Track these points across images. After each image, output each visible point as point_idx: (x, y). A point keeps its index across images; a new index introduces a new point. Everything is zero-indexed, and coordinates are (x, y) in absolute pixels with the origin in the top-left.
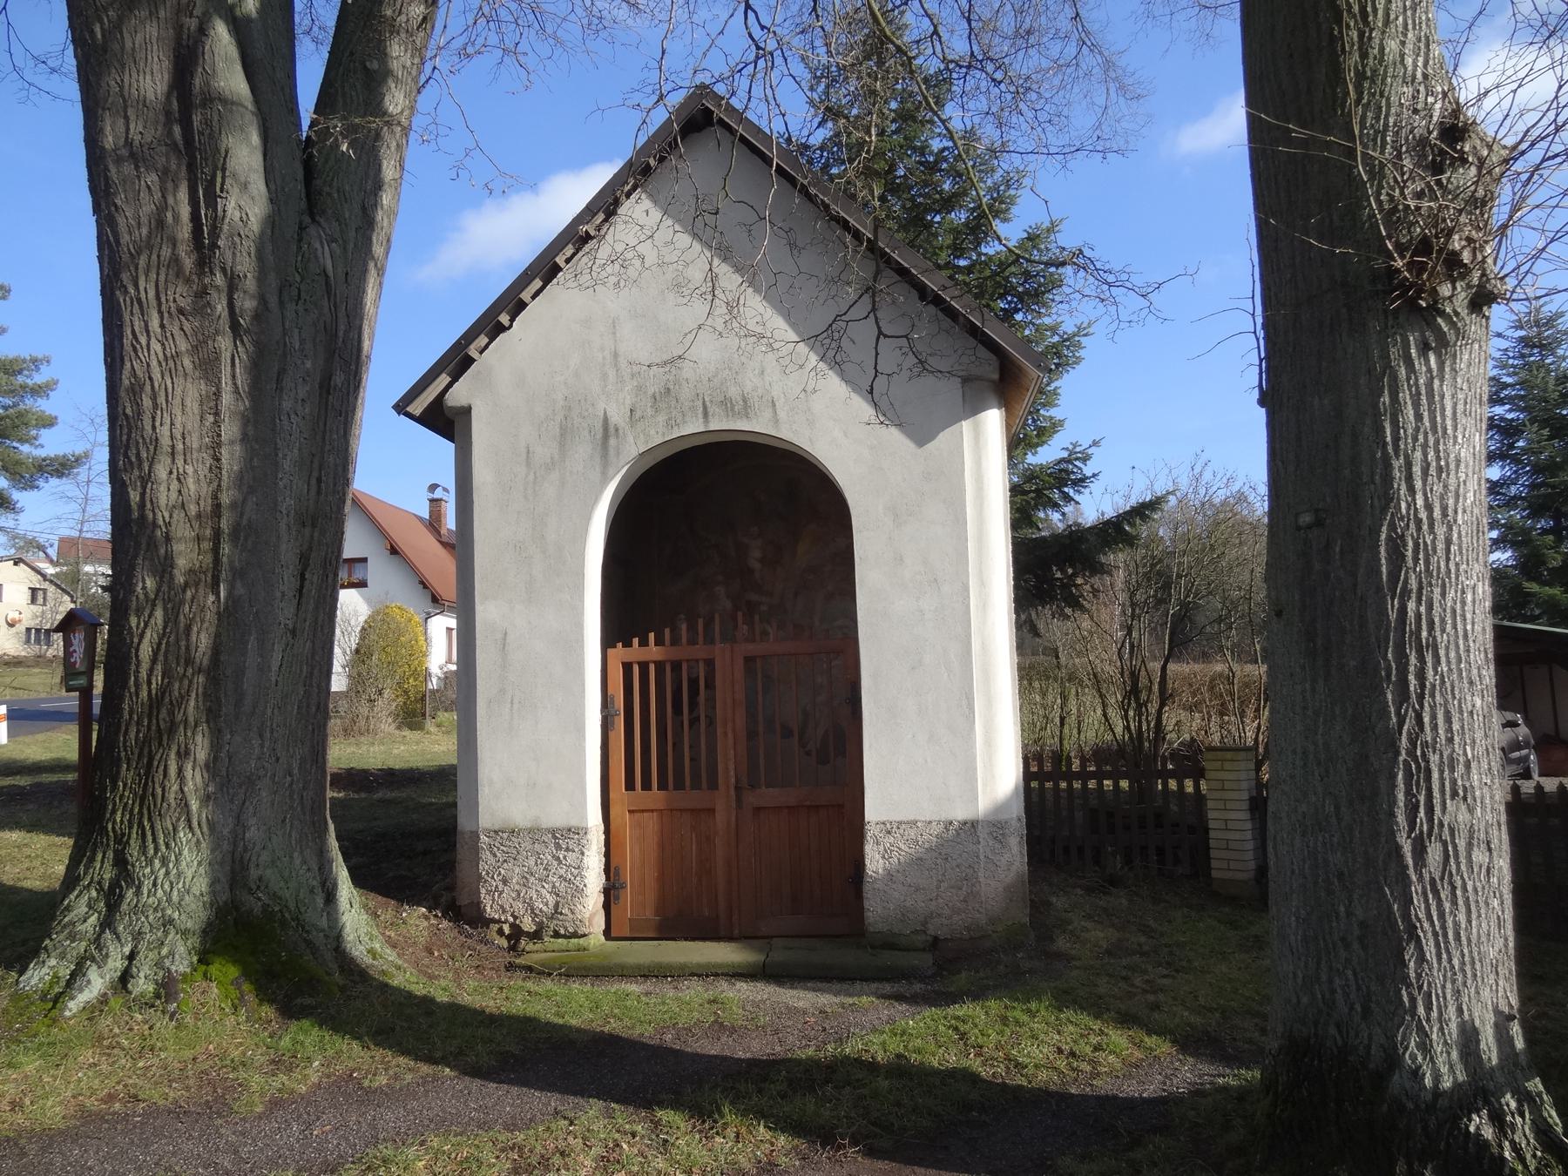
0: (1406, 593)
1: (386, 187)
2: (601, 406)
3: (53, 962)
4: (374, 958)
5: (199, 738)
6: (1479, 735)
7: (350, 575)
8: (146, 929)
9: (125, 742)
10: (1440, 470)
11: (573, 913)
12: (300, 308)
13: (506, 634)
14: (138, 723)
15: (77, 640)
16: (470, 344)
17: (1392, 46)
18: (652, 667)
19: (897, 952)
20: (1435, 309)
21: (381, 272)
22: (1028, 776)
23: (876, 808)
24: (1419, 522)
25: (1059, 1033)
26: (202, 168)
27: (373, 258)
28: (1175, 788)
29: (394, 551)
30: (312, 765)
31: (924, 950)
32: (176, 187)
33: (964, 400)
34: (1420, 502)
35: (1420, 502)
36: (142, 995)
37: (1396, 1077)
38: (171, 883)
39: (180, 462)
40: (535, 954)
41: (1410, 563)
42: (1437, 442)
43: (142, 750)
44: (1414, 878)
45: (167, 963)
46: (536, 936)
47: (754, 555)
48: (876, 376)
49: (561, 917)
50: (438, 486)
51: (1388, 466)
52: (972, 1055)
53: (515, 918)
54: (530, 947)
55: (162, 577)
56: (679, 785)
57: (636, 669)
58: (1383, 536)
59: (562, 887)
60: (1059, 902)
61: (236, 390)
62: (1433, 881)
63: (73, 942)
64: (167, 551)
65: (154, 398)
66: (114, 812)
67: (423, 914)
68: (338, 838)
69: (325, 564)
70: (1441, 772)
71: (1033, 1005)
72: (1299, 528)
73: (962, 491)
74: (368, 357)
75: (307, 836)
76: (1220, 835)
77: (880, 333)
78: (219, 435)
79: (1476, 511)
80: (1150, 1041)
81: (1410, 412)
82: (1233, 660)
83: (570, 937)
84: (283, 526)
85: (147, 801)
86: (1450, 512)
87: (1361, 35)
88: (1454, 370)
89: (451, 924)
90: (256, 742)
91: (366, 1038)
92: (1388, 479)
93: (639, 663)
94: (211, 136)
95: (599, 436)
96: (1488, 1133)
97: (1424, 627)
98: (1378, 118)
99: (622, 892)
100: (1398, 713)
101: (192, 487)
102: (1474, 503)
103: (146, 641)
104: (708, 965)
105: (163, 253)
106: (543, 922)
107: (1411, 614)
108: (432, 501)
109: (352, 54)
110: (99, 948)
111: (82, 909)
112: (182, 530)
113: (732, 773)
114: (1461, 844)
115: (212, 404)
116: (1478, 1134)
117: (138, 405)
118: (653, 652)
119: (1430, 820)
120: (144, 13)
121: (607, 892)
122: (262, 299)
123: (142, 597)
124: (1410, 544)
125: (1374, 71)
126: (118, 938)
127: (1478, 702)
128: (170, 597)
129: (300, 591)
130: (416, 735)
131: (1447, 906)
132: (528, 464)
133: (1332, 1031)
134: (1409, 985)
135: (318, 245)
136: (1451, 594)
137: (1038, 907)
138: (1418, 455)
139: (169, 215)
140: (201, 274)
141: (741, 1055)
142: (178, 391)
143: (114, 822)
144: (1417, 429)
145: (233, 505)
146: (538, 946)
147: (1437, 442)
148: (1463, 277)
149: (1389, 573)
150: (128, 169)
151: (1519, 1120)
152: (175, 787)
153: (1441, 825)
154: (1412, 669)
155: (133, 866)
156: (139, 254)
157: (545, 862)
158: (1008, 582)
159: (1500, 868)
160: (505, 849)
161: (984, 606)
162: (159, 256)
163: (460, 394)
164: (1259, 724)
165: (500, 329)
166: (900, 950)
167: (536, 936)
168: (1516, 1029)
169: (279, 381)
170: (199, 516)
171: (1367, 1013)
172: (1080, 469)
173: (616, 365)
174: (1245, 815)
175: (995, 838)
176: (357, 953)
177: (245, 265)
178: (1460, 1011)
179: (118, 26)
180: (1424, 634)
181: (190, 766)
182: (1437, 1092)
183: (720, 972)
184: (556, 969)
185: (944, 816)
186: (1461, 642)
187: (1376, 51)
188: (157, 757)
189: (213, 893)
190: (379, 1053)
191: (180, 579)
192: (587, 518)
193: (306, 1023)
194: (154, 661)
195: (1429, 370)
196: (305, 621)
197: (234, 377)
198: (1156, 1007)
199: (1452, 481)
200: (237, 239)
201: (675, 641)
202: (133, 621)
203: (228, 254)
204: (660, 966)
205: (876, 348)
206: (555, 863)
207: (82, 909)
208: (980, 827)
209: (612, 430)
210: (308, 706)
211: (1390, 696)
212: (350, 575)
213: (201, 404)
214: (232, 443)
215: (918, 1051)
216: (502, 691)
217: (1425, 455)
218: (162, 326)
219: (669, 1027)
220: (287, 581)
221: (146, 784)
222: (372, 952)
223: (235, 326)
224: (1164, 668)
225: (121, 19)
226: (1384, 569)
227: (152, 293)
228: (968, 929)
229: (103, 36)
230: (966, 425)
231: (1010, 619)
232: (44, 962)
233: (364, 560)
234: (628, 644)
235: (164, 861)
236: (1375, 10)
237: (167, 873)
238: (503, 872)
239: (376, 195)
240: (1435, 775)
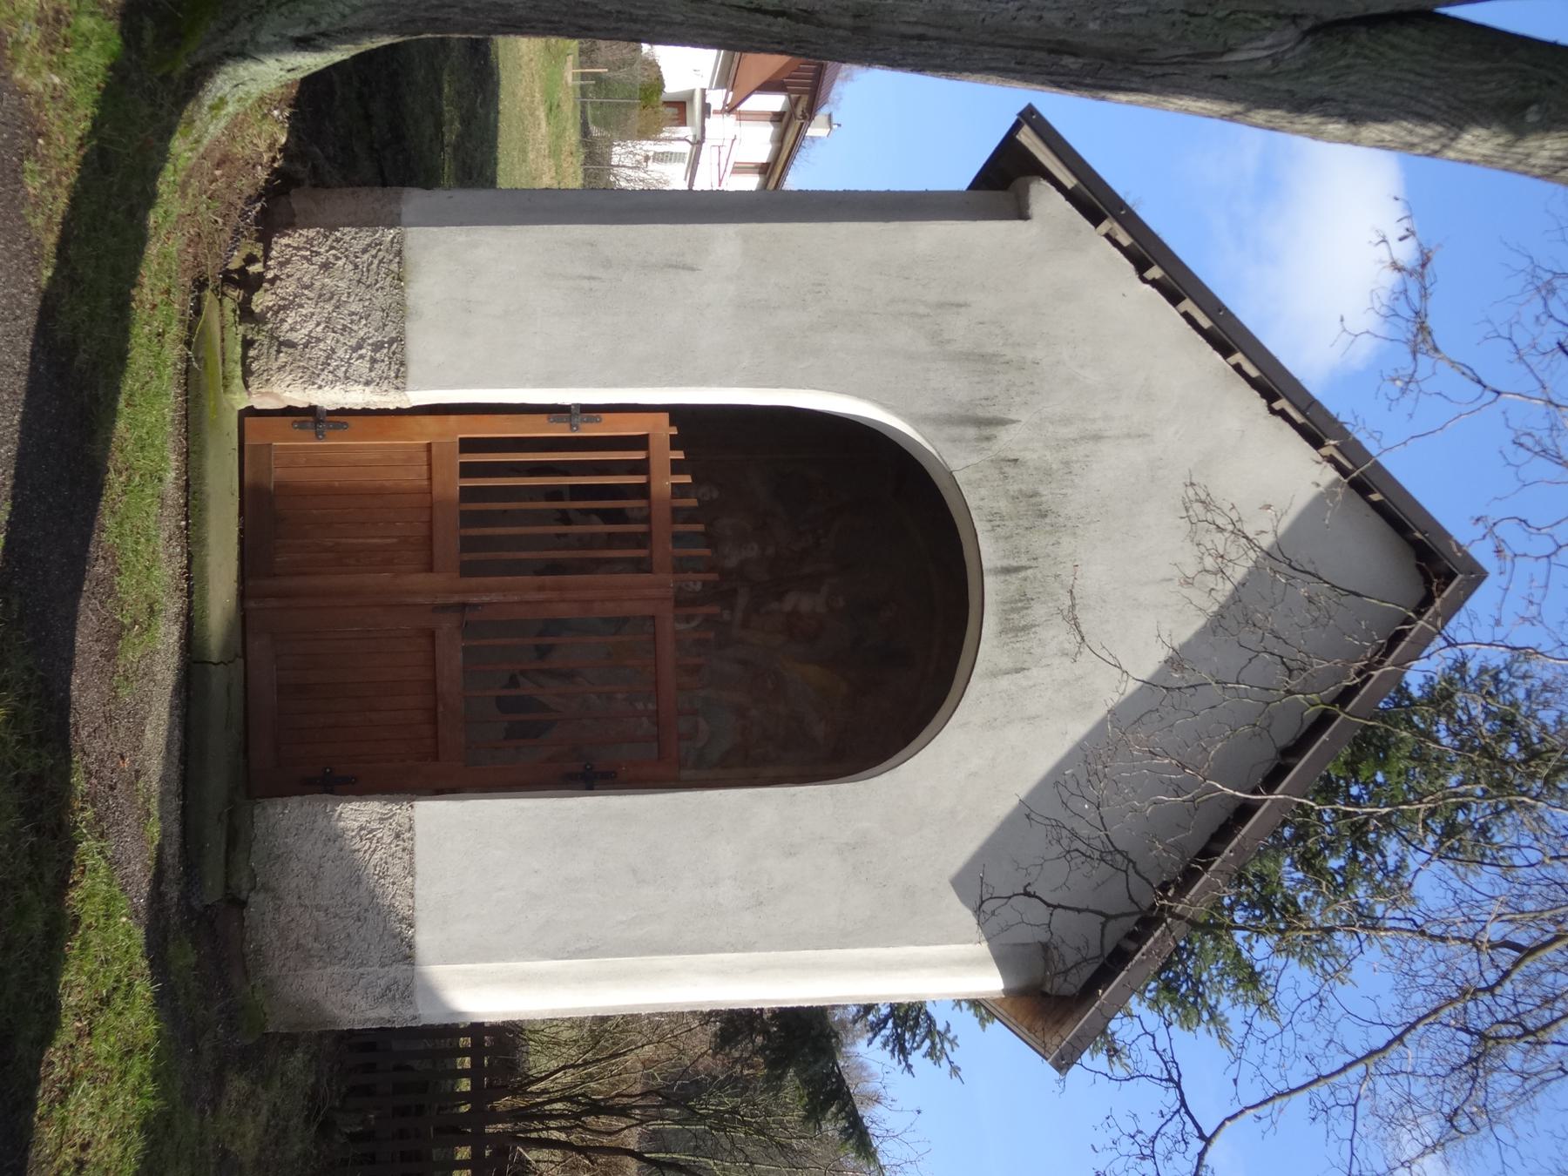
1: (1352, 128)
2: (1024, 416)
4: (211, 108)
11: (279, 369)
12: (1177, 17)
13: (693, 269)
16: (1120, 223)
18: (640, 479)
19: (223, 846)
21: (1230, 117)
22: (477, 1029)
25: (111, 1136)
27: (1249, 110)
30: (499, 19)
31: (227, 887)
33: (1015, 945)
40: (220, 312)
46: (246, 313)
47: (804, 603)
48: (1049, 905)
49: (273, 351)
52: (78, 1024)
53: (272, 281)
54: (229, 304)
56: (468, 519)
57: (639, 455)
59: (318, 352)
60: (298, 1059)
67: (276, 140)
68: (392, 46)
69: (799, 42)
71: (149, 1088)
74: (1103, 99)
75: (393, 13)
77: (1108, 917)
83: (243, 364)
89: (262, 183)
91: (94, 142)
93: (647, 460)
104: (203, 581)
106: (266, 323)
109: (1551, 83)
113: (486, 599)
118: (663, 482)
121: (312, 410)
129: (759, 10)
132: (941, 305)
135: (1268, 41)
137: (289, 1041)
141: (76, 681)
146: (230, 317)
157: (355, 328)
158: (756, 1001)
160: (374, 266)
161: (723, 972)
163: (1047, 202)
165: (1141, 266)
166: (227, 852)
167: (246, 313)
172: (919, 1047)
173: (1082, 438)
175: (388, 988)
176: (219, 82)
183: (194, 597)
184: (196, 352)
185: (421, 917)
190: (72, 164)
192: (860, 395)
193: (116, 44)
196: (714, 15)
204: (202, 509)
205: (1087, 910)
206: (353, 342)
208: (405, 967)
209: (987, 431)
210: (587, 16)
215: (85, 945)
216: (607, 264)
219: (115, 563)
222: (223, 101)
228: (258, 951)
230: (983, 949)
231: (700, 1004)
234: (675, 443)
238: (340, 263)
239: (1341, 116)
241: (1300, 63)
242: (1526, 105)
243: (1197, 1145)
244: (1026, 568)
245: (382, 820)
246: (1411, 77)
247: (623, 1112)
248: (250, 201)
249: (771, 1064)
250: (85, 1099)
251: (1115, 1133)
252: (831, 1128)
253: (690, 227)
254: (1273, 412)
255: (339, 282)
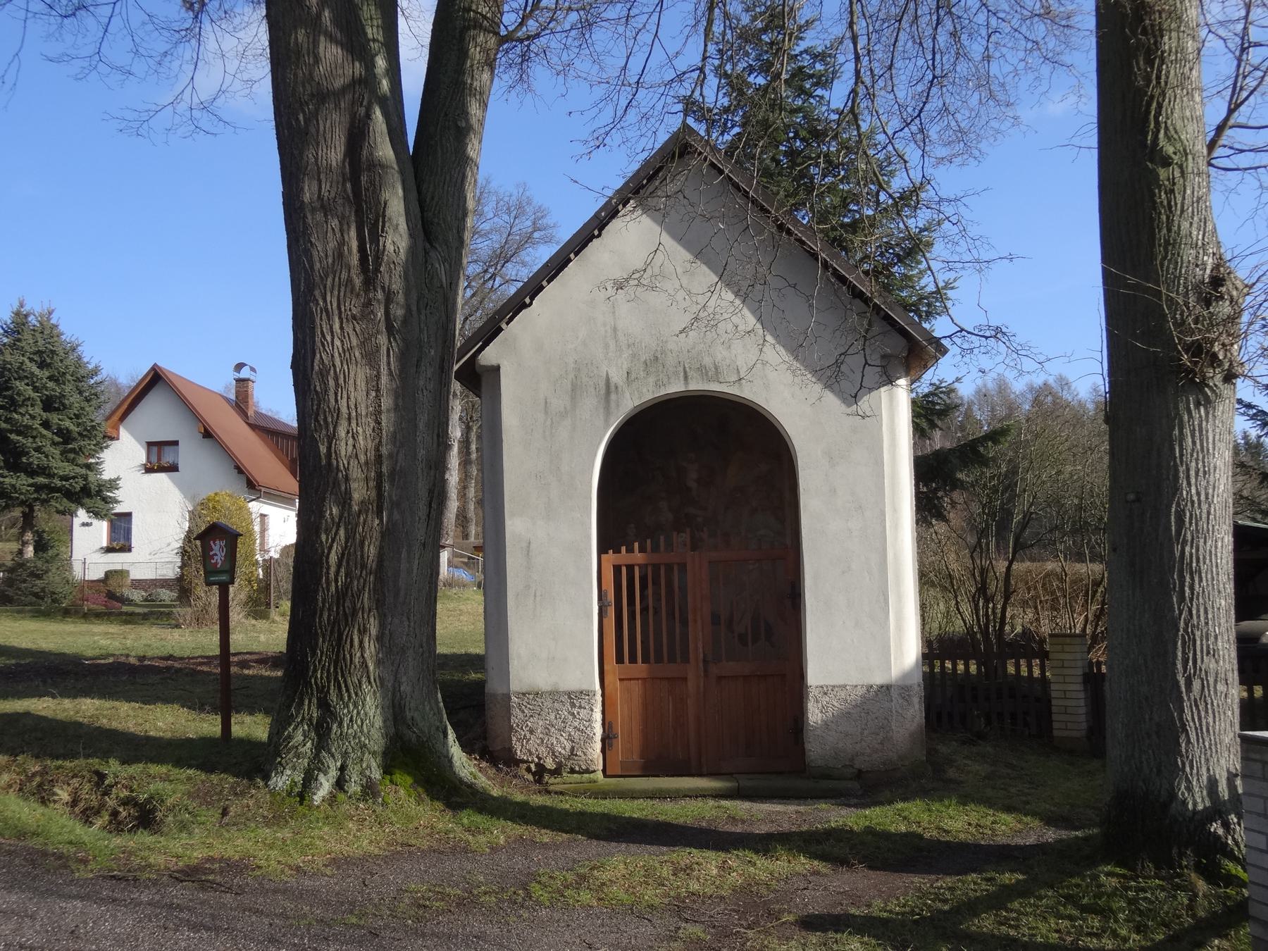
0: (1185, 542)
2: (604, 369)
3: (289, 772)
5: (372, 620)
6: (1223, 621)
7: (159, 459)
8: (350, 750)
9: (320, 622)
10: (1205, 472)
14: (329, 609)
15: (218, 546)
17: (1185, 225)
20: (1204, 383)
23: (816, 675)
24: (1193, 502)
26: (367, 214)
28: (1013, 672)
29: (208, 434)
31: (851, 779)
32: (349, 227)
34: (1194, 491)
35: (1194, 491)
36: (355, 793)
37: (1174, 805)
38: (362, 720)
39: (354, 425)
41: (1187, 525)
42: (1204, 457)
43: (333, 628)
44: (1185, 698)
45: (368, 773)
46: (556, 772)
50: (246, 365)
51: (1177, 471)
53: (540, 759)
54: (552, 780)
55: (343, 507)
56: (659, 659)
57: (624, 570)
58: (1173, 510)
59: (576, 735)
60: (943, 749)
61: (390, 373)
62: (1195, 700)
63: (298, 759)
64: (346, 488)
65: (336, 379)
66: (315, 671)
70: (1202, 641)
72: (1127, 502)
73: (881, 441)
76: (1060, 702)
77: (866, 363)
78: (380, 406)
79: (1225, 495)
80: (1028, 819)
81: (1189, 440)
82: (1065, 561)
84: (420, 471)
85: (340, 663)
86: (1210, 497)
87: (1168, 218)
88: (1214, 416)
90: (406, 623)
92: (1176, 477)
93: (626, 566)
94: (374, 192)
95: (603, 392)
96: (1221, 832)
97: (1194, 561)
98: (1175, 269)
99: (614, 741)
100: (1179, 608)
101: (362, 442)
102: (1224, 491)
103: (333, 552)
105: (342, 276)
107: (1187, 554)
108: (239, 381)
110: (320, 761)
111: (299, 737)
112: (356, 473)
114: (1211, 680)
115: (374, 383)
116: (1215, 832)
117: (326, 384)
118: (638, 557)
119: (1195, 667)
120: (332, 106)
121: (603, 740)
122: (408, 308)
123: (329, 520)
124: (1188, 514)
125: (1175, 240)
126: (333, 756)
127: (1223, 603)
128: (348, 520)
130: (261, 624)
131: (1203, 714)
132: (546, 413)
133: (1141, 784)
134: (1182, 756)
136: (1209, 543)
138: (1193, 464)
139: (346, 248)
140: (367, 291)
142: (352, 375)
143: (316, 678)
144: (1193, 450)
145: (390, 456)
147: (1204, 457)
148: (1219, 366)
149: (1176, 531)
150: (319, 216)
151: (1238, 827)
152: (358, 654)
153: (1201, 670)
154: (1187, 584)
155: (335, 708)
156: (327, 277)
159: (1233, 695)
161: (896, 526)
162: (340, 279)
163: (489, 356)
164: (1087, 616)
165: (525, 306)
167: (556, 772)
168: (1238, 782)
169: (417, 366)
170: (367, 463)
171: (1159, 771)
174: (1080, 687)
175: (903, 698)
177: (397, 285)
178: (1208, 770)
179: (315, 115)
180: (1194, 565)
181: (367, 640)
182: (1195, 812)
186: (1214, 569)
187: (1176, 228)
188: (345, 633)
189: (385, 726)
191: (356, 508)
194: (339, 566)
195: (1201, 417)
197: (389, 363)
198: (1027, 803)
199: (1212, 479)
200: (392, 266)
201: (655, 549)
202: (324, 537)
203: (387, 276)
206: (571, 717)
207: (299, 737)
209: (613, 388)
211: (1175, 599)
212: (159, 459)
213: (367, 383)
214: (388, 411)
215: (878, 824)
217: (1197, 464)
218: (342, 328)
220: (422, 511)
221: (338, 651)
223: (390, 330)
224: (1009, 568)
225: (317, 111)
226: (1173, 528)
227: (335, 305)
229: (305, 122)
232: (282, 772)
233: (176, 443)
234: (617, 551)
235: (355, 706)
236: (1176, 204)
237: (358, 713)
240: (1198, 643)
241: (445, 247)
242: (458, 127)
243: (964, 333)
244: (684, 368)
245: (817, 702)
246: (446, 187)
247: (984, 572)
248: (499, 770)
249: (954, 488)
250: (948, 824)
251: (962, 364)
252: (991, 451)
253: (507, 544)
254: (599, 235)
255: (539, 725)
